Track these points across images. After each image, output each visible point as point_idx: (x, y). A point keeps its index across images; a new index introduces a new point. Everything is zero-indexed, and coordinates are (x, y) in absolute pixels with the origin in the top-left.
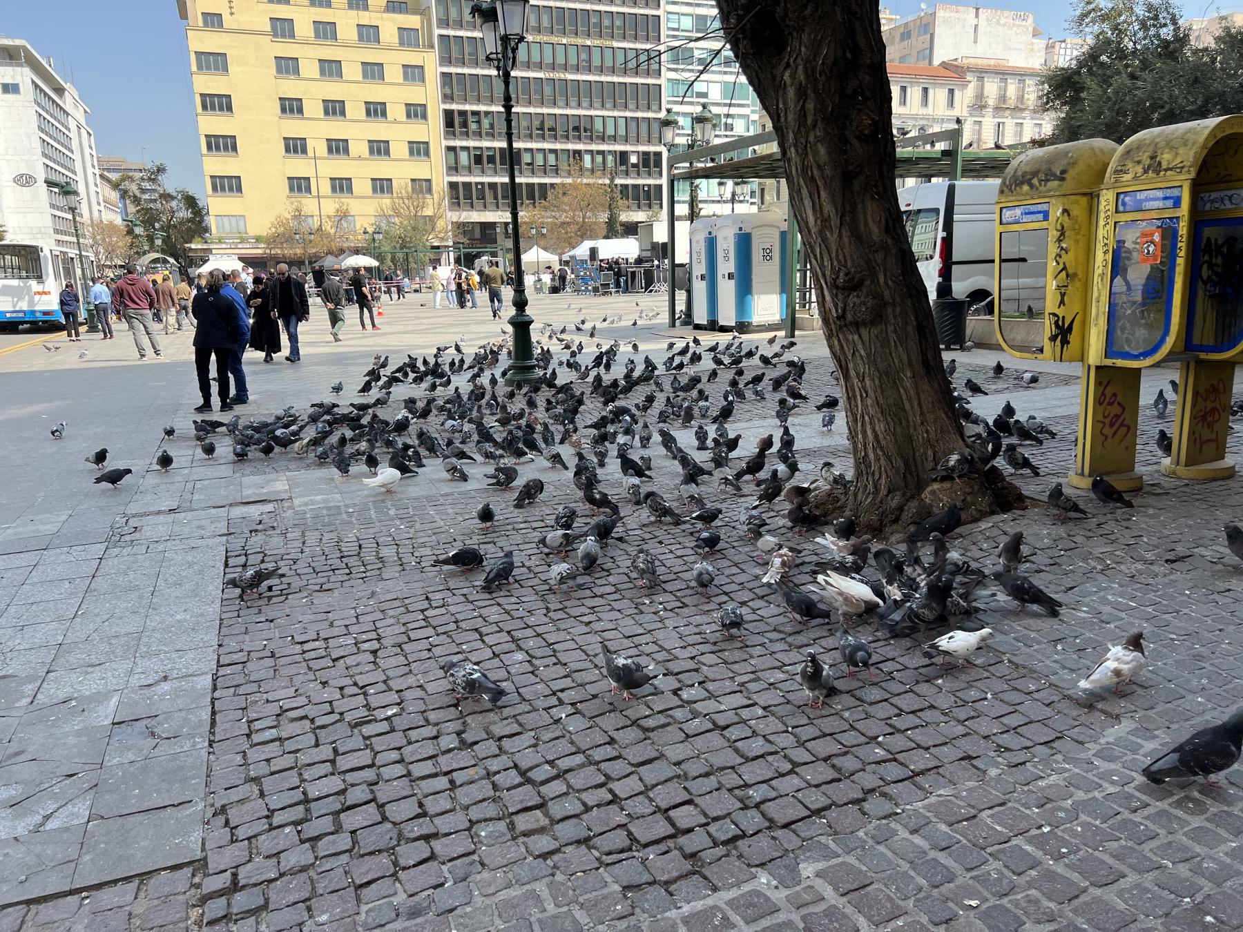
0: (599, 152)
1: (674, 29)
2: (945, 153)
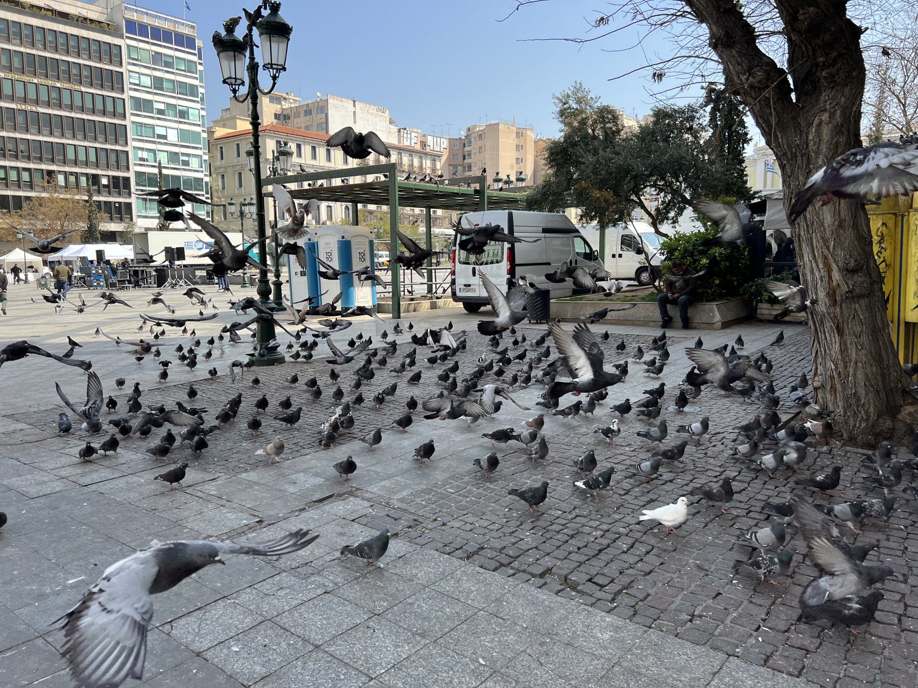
0: (71, 173)
1: (135, 84)
2: (477, 192)
